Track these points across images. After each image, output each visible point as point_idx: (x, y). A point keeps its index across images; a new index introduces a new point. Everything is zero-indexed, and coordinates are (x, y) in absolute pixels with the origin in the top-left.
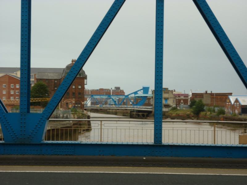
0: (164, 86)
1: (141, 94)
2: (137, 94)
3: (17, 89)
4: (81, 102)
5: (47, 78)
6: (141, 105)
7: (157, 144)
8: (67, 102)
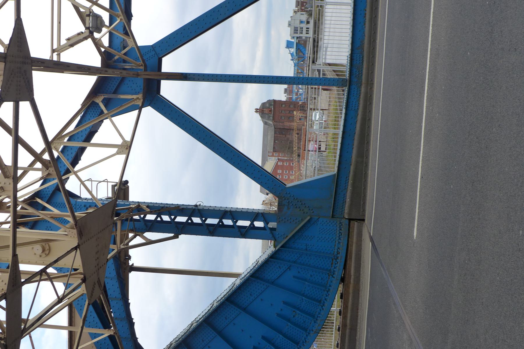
0: (285, 100)
1: (293, 50)
2: (293, 53)
3: (283, 172)
4: (299, 105)
5: (273, 141)
6: (305, 50)
7: (346, 85)
8: (299, 120)
